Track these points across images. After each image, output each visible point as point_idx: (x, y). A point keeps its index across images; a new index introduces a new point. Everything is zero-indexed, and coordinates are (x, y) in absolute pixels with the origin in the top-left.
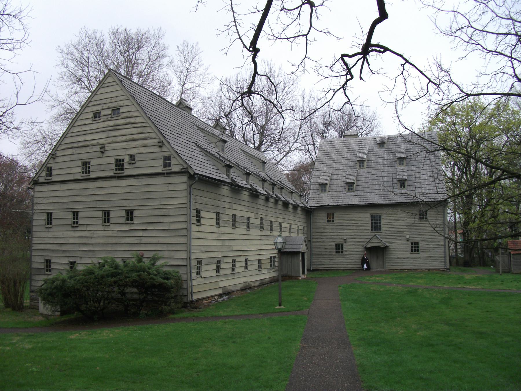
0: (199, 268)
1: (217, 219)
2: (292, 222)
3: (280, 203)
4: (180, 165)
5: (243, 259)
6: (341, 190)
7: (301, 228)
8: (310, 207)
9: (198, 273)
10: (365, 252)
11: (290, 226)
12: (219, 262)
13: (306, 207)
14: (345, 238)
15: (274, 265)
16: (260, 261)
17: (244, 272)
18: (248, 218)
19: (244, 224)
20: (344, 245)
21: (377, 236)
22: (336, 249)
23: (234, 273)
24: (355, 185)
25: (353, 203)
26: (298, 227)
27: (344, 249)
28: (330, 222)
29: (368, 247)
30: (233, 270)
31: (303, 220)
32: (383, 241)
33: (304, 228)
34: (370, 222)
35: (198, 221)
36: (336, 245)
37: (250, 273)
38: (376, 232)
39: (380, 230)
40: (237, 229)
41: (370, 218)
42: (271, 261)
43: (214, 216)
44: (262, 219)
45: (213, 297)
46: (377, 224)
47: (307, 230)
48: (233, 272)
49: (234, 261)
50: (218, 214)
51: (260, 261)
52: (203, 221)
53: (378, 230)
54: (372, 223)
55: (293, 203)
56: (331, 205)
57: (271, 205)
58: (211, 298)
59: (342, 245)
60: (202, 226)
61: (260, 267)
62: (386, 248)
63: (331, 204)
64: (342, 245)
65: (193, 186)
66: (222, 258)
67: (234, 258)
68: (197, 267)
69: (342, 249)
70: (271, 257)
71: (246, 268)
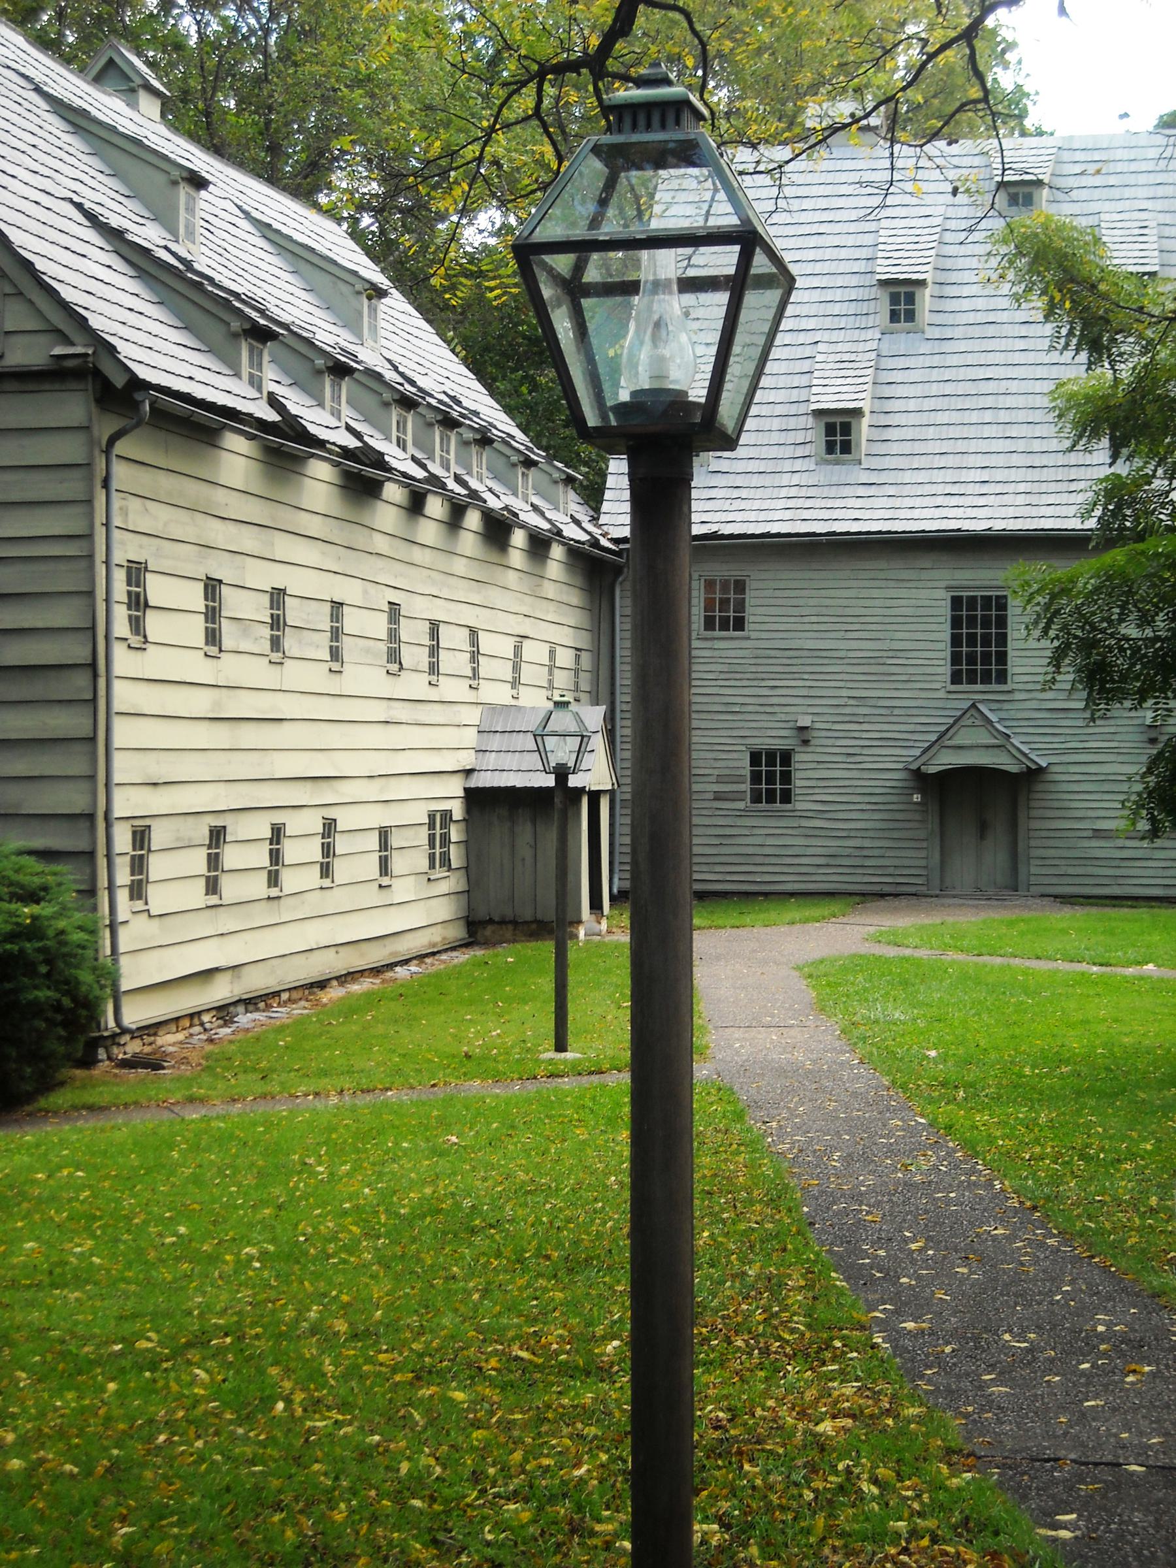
0: (138, 865)
1: (212, 614)
2: (526, 627)
3: (473, 519)
4: (43, 339)
5: (261, 827)
6: (788, 452)
7: (565, 658)
8: (612, 540)
9: (137, 891)
10: (917, 798)
11: (518, 650)
12: (217, 836)
13: (595, 543)
14: (805, 721)
15: (446, 861)
16: (384, 834)
17: (318, 893)
18: (337, 607)
19: (316, 635)
20: (797, 757)
21: (981, 707)
22: (756, 778)
23: (279, 898)
24: (865, 421)
25: (855, 527)
26: (552, 653)
27: (799, 781)
28: (724, 626)
29: (932, 770)
30: (274, 879)
31: (574, 617)
32: (1015, 741)
33: (578, 657)
34: (946, 634)
35: (137, 625)
36: (755, 758)
37: (338, 899)
38: (979, 687)
39: (1002, 677)
40: (288, 662)
41: (945, 610)
42: (432, 838)
43: (195, 597)
44: (394, 611)
45: (194, 1016)
46: (986, 623)
47: (595, 671)
48: (274, 892)
49: (277, 833)
50: (212, 587)
51: (384, 834)
52: (153, 622)
53: (986, 679)
54: (956, 640)
55: (533, 519)
56: (731, 536)
57: (429, 531)
58: (187, 1023)
59: (786, 757)
60: (151, 649)
61: (384, 867)
62: (1034, 774)
63: (727, 530)
64: (786, 757)
65: (120, 448)
66: (229, 816)
67: (278, 817)
68: (133, 857)
69: (787, 777)
70: (432, 816)
71: (326, 870)
